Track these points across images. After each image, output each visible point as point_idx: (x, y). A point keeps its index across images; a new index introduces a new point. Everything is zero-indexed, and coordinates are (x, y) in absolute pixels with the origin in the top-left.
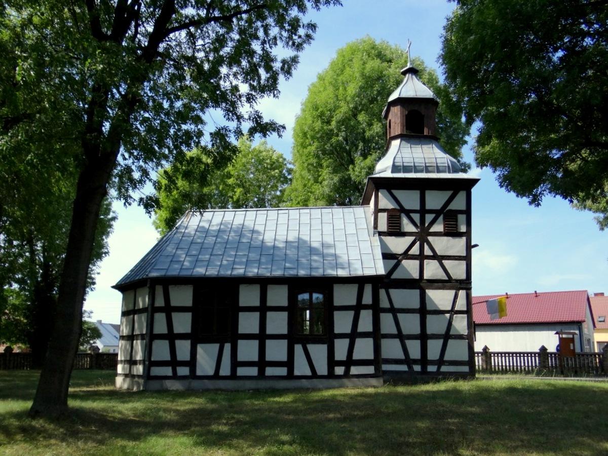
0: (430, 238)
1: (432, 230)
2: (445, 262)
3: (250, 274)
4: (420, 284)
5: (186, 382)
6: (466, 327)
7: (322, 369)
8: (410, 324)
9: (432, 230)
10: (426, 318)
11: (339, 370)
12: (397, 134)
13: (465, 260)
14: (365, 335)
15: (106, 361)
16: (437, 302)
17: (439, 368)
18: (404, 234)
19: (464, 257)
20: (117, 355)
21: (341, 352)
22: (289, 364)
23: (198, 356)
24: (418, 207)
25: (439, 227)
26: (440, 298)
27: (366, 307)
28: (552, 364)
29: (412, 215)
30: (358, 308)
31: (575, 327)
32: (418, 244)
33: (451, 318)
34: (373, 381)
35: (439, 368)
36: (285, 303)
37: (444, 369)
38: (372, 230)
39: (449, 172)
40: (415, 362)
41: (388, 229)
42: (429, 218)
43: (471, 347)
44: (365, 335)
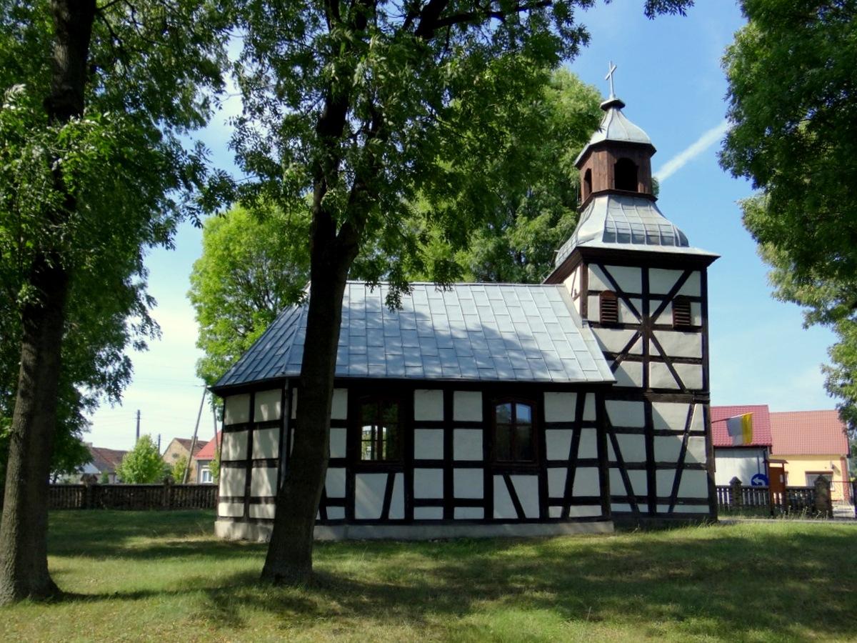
0: (656, 333)
1: (658, 322)
2: (676, 366)
3: (432, 376)
4: (643, 395)
5: (341, 529)
6: (705, 454)
7: (532, 510)
8: (633, 448)
9: (658, 322)
10: (653, 440)
11: (555, 512)
12: (602, 189)
13: (700, 363)
14: (587, 463)
15: (108, 497)
17: (671, 508)
18: (622, 326)
19: (699, 359)
20: (216, 487)
21: (556, 488)
22: (487, 502)
23: (358, 492)
24: (639, 290)
25: (667, 318)
26: (671, 414)
27: (589, 425)
28: (747, 502)
29: (632, 300)
30: (577, 426)
31: (759, 452)
32: (640, 340)
33: (685, 440)
34: (601, 526)
35: (671, 508)
36: (478, 417)
37: (678, 509)
38: (580, 320)
39: (677, 245)
40: (641, 499)
41: (601, 318)
42: (654, 305)
43: (711, 481)
44: (587, 463)
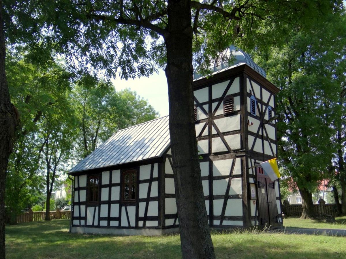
0: (215, 121)
2: (226, 138)
6: (241, 189)
7: (133, 224)
9: (216, 115)
10: (212, 183)
11: (104, 223)
16: (220, 170)
17: (221, 222)
21: (104, 213)
25: (221, 111)
35: (221, 222)
44: (219, 197)
